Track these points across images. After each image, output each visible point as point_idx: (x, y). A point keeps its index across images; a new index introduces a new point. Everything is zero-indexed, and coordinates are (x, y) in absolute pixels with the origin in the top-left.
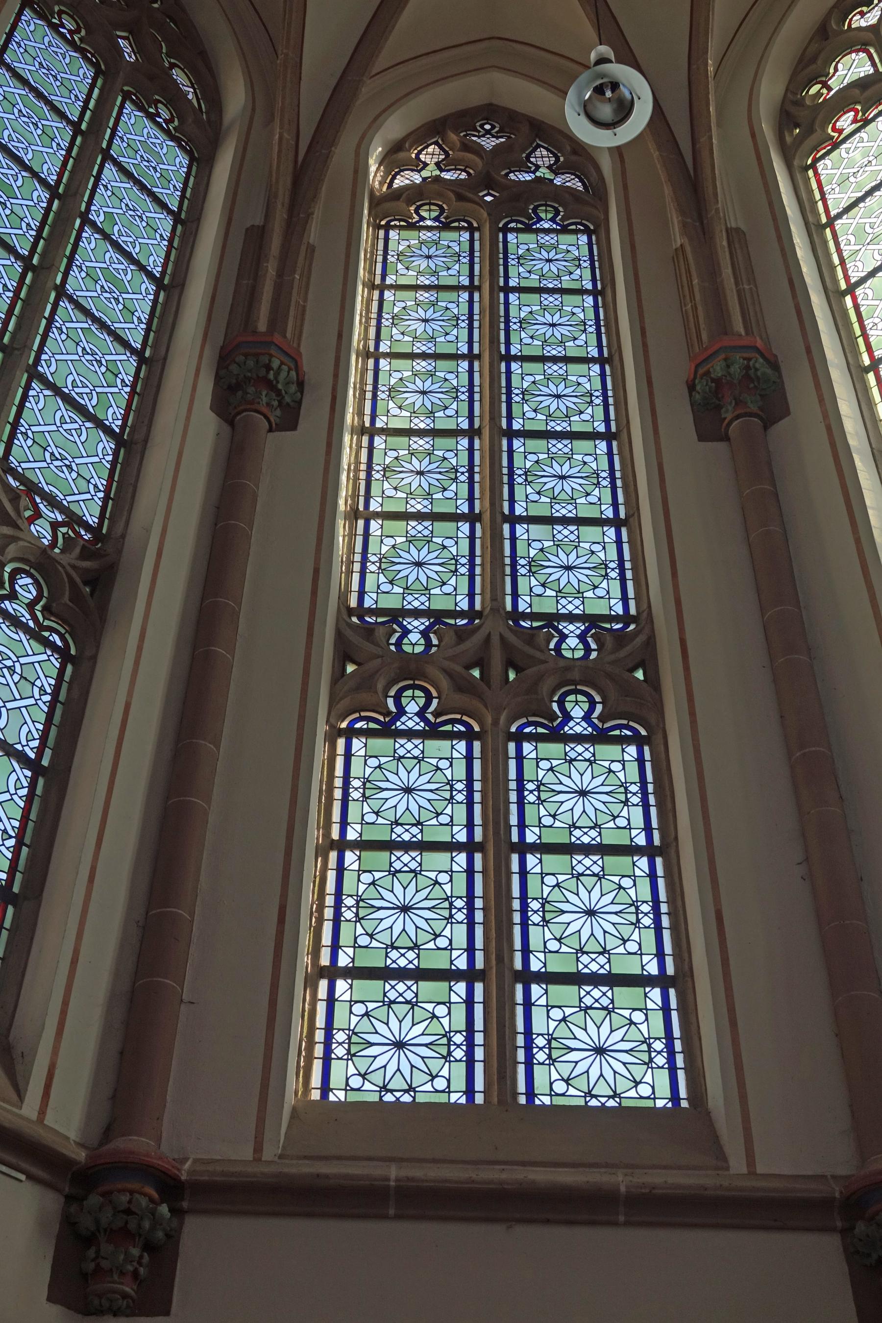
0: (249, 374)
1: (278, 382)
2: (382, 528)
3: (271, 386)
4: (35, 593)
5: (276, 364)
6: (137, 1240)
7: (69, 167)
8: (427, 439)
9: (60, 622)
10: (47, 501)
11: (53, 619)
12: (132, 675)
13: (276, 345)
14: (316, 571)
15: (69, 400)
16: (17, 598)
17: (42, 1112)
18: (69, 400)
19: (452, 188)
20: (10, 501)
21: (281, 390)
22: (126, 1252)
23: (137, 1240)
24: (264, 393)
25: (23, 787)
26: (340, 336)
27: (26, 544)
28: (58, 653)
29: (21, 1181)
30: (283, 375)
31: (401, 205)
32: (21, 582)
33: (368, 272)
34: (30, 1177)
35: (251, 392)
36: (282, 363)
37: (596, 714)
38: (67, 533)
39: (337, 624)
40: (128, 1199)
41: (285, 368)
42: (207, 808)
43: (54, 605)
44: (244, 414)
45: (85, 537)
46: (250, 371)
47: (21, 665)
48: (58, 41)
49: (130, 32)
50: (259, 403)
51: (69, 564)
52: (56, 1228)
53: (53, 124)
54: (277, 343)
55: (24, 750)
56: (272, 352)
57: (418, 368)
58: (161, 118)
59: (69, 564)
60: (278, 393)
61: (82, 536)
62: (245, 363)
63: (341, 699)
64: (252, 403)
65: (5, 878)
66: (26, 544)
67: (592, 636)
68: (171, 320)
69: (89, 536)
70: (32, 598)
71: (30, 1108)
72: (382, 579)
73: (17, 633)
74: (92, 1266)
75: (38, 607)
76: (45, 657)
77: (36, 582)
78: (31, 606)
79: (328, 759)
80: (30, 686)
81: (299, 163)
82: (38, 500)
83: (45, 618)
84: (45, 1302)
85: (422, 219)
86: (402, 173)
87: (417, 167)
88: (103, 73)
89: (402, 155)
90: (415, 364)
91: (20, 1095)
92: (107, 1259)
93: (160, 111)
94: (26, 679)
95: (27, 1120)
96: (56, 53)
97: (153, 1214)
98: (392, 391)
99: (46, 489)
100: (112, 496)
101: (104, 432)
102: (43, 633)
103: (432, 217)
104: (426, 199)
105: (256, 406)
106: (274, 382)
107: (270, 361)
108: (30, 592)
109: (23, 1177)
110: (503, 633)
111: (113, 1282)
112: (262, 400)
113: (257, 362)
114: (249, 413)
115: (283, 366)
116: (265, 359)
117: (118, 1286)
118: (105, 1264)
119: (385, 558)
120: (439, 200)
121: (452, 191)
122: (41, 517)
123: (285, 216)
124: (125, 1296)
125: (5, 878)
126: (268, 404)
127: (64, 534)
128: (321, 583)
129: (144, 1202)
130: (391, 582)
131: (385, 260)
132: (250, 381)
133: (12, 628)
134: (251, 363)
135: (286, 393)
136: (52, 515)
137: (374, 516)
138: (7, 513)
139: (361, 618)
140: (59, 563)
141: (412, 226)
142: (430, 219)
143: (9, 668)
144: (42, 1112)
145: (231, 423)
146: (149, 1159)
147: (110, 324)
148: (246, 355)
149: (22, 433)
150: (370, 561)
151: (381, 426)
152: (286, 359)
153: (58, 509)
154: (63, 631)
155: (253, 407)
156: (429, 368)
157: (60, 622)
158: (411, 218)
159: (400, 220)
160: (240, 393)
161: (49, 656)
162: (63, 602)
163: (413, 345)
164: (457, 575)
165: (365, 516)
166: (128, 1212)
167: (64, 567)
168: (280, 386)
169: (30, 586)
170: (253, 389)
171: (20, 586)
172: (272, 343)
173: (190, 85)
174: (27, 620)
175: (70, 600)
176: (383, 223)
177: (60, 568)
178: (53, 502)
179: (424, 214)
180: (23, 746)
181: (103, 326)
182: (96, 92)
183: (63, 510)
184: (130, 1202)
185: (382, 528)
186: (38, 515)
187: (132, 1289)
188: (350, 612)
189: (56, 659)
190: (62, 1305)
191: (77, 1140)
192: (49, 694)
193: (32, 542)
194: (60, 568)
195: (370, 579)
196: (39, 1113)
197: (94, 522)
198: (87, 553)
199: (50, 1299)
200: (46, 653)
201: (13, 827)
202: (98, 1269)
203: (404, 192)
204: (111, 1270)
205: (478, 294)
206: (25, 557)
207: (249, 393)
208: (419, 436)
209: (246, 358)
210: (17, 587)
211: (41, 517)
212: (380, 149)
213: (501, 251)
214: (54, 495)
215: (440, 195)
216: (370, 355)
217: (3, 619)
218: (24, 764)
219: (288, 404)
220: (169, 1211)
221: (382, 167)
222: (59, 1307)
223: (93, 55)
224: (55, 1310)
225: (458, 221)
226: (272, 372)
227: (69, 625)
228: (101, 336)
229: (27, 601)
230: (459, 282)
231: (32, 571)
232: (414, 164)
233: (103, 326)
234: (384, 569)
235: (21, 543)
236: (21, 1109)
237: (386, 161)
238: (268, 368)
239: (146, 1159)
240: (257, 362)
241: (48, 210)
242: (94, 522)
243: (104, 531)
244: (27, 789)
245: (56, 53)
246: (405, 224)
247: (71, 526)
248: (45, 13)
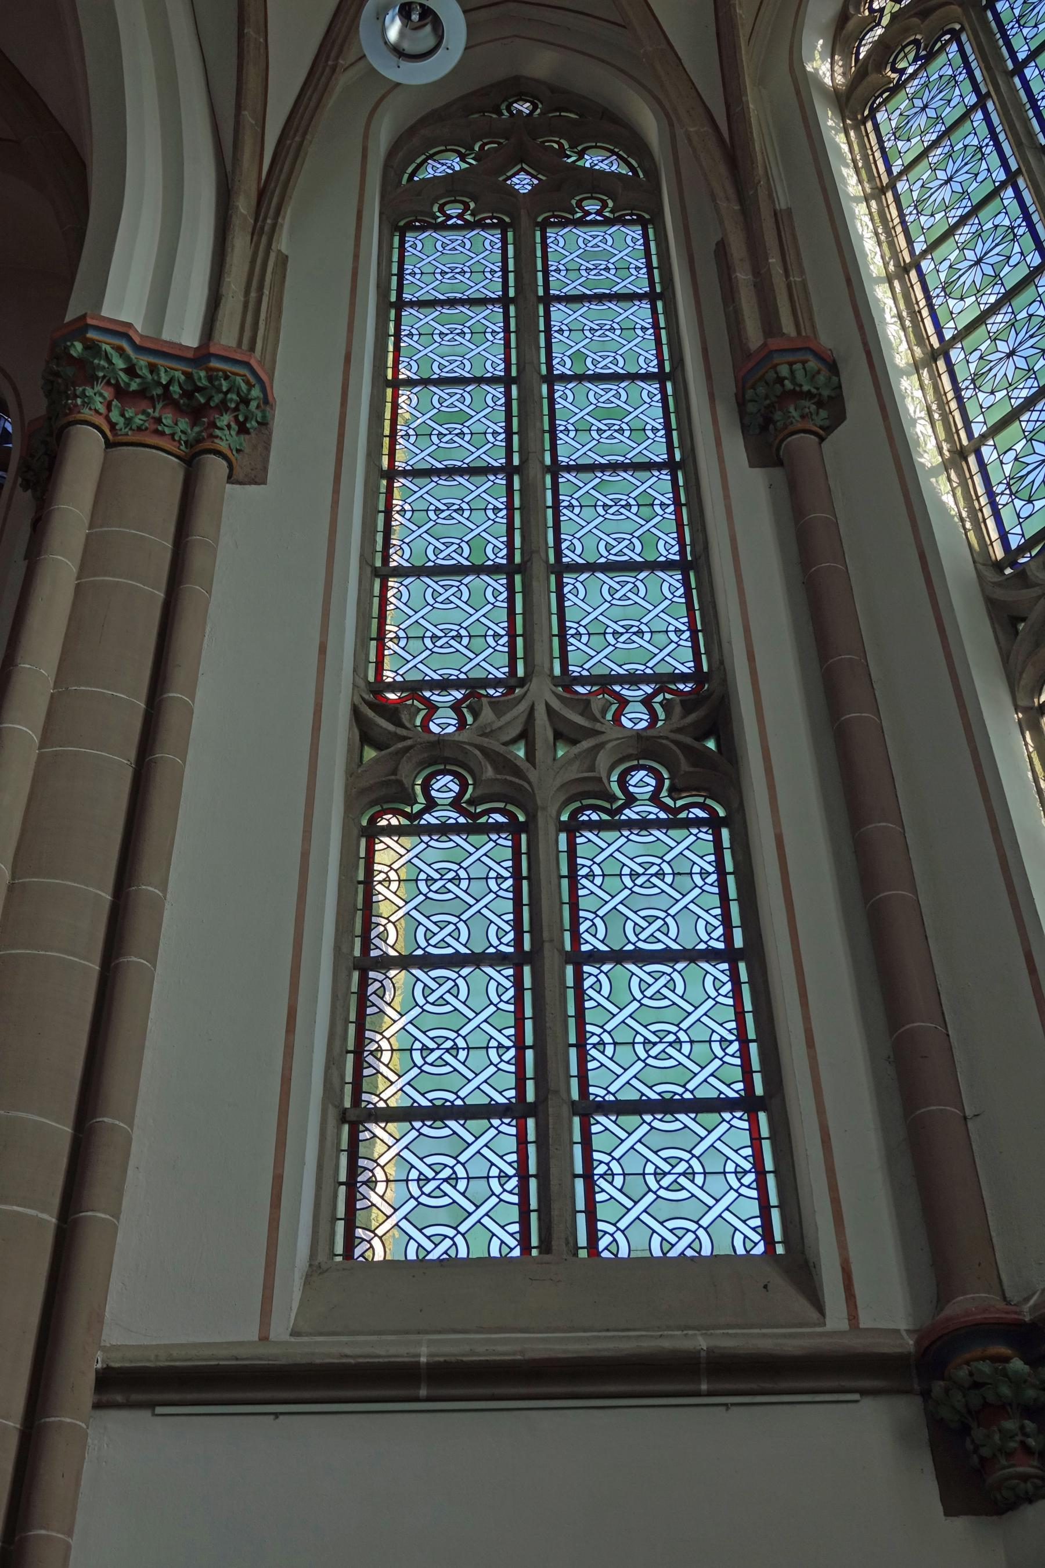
0: (768, 402)
1: (801, 386)
2: (995, 448)
3: (797, 395)
4: (653, 782)
5: (784, 370)
6: (1009, 1410)
7: (513, 344)
8: (1003, 311)
9: (694, 793)
10: (627, 683)
11: (684, 795)
12: (771, 804)
13: (776, 350)
14: (922, 556)
15: (609, 567)
16: (637, 800)
17: (853, 1317)
18: (609, 567)
19: (912, 12)
20: (582, 714)
21: (809, 391)
22: (1000, 1431)
23: (1009, 1410)
24: (792, 409)
25: (724, 984)
26: (849, 281)
27: (615, 743)
28: (704, 825)
29: (856, 1401)
30: (800, 375)
31: (873, 78)
32: (633, 782)
33: (869, 181)
34: (864, 1392)
35: (779, 418)
36: (791, 364)
37: (467, 796)
38: (664, 698)
39: (983, 590)
40: (967, 1372)
41: (798, 366)
42: (129, 1130)
43: (676, 781)
44: (783, 446)
45: (687, 689)
46: (767, 397)
47: (668, 863)
48: (452, 235)
49: (522, 161)
50: (792, 423)
51: (672, 731)
52: (925, 1434)
53: (478, 318)
54: (775, 348)
55: (709, 946)
56: (776, 361)
57: (962, 239)
58: (591, 214)
59: (672, 731)
60: (809, 395)
61: (682, 691)
62: (756, 393)
63: (1021, 674)
64: (786, 427)
65: (592, 1127)
66: (615, 743)
67: (467, 707)
68: (684, 406)
69: (690, 685)
70: (653, 789)
71: (836, 1319)
72: (1018, 503)
73: (651, 834)
74: (975, 1459)
75: (664, 793)
76: (692, 838)
77: (651, 770)
78: (655, 799)
79: (1036, 748)
80: (688, 878)
81: (728, 140)
82: (617, 688)
83: (675, 800)
84: (944, 1518)
85: (902, 71)
86: (864, 42)
87: (875, 21)
88: (510, 225)
89: (851, 25)
90: (957, 237)
91: (821, 1310)
92: (984, 1445)
93: (586, 208)
94: (679, 874)
95: (842, 1333)
96: (454, 249)
97: (1006, 1375)
98: (946, 288)
99: (622, 672)
100: (699, 628)
101: (662, 571)
102: (679, 817)
103: (911, 62)
104: (897, 46)
105: (791, 428)
106: (798, 389)
107: (776, 373)
108: (648, 785)
109: (856, 1397)
110: (548, 701)
111: (1004, 1468)
112: (794, 417)
113: (767, 383)
114: (785, 443)
115: (794, 366)
116: (771, 375)
117: (1011, 1470)
118: (985, 1452)
119: (1013, 478)
120: (910, 36)
121: (911, 17)
122: (628, 702)
123: (737, 207)
124: (1025, 1478)
125: (592, 1127)
126: (803, 417)
127: (661, 703)
128: (932, 568)
129: (986, 1367)
130: (1030, 501)
131: (882, 149)
132: (774, 407)
133: (644, 833)
134: (761, 390)
135: (817, 389)
136: (641, 693)
137: (981, 441)
138: (582, 727)
139: (1013, 564)
140: (660, 737)
141: (900, 86)
142: (910, 65)
143: (656, 875)
144: (853, 1317)
145: (779, 463)
146: (970, 1318)
147: (622, 459)
148: (753, 387)
149: (572, 636)
150: (998, 494)
151: (951, 336)
152: (791, 358)
153: (642, 682)
154: (701, 800)
155: (786, 432)
156: (974, 229)
157: (694, 793)
158: (890, 83)
159: (881, 95)
160: (771, 427)
161: (695, 835)
162: (682, 773)
163: (947, 218)
164: (1006, 478)
165: (972, 448)
166: (976, 1385)
167: (667, 738)
168: (806, 388)
169: (647, 779)
170: (779, 413)
171: (635, 786)
172: (771, 352)
173: (609, 154)
174: (656, 814)
175: (694, 765)
176: (866, 113)
177: (664, 741)
178: (633, 679)
179: (901, 65)
180: (706, 943)
181: (614, 467)
182: (511, 249)
183: (645, 679)
184: (971, 1374)
185: (995, 448)
186: (624, 702)
187: (1033, 1467)
188: (999, 566)
189: (706, 833)
190: (966, 1514)
191: (911, 1327)
192: (713, 873)
193: (620, 736)
194: (664, 741)
195: (1006, 514)
196: (849, 1320)
197: (689, 668)
198: (689, 703)
199: (948, 1512)
200: (691, 834)
201: (730, 1031)
202: (983, 1460)
203: (868, 63)
204: (994, 1455)
205: (991, 102)
206: (625, 754)
207: (778, 421)
208: (994, 314)
209: (755, 390)
210: (631, 789)
211: (628, 702)
212: (821, 42)
213: (996, 30)
214: (632, 671)
215: (907, 31)
216: (908, 268)
217: (629, 830)
218: (715, 959)
219: (829, 397)
220: (1026, 1363)
221: (836, 57)
222: (966, 1517)
223: (491, 218)
224: (960, 1524)
225: (939, 39)
226: (786, 382)
227: (704, 790)
228: (619, 478)
229: (647, 796)
230: (966, 106)
231: (642, 762)
232: (870, 20)
233: (614, 467)
234: (1017, 492)
235: (609, 746)
236: (825, 1325)
237: (838, 47)
238: (780, 380)
239: (967, 1319)
240: (767, 383)
241: (508, 404)
242: (689, 668)
243: (705, 669)
244: (730, 983)
245: (454, 249)
246: (887, 94)
247: (666, 689)
248: (425, 221)
